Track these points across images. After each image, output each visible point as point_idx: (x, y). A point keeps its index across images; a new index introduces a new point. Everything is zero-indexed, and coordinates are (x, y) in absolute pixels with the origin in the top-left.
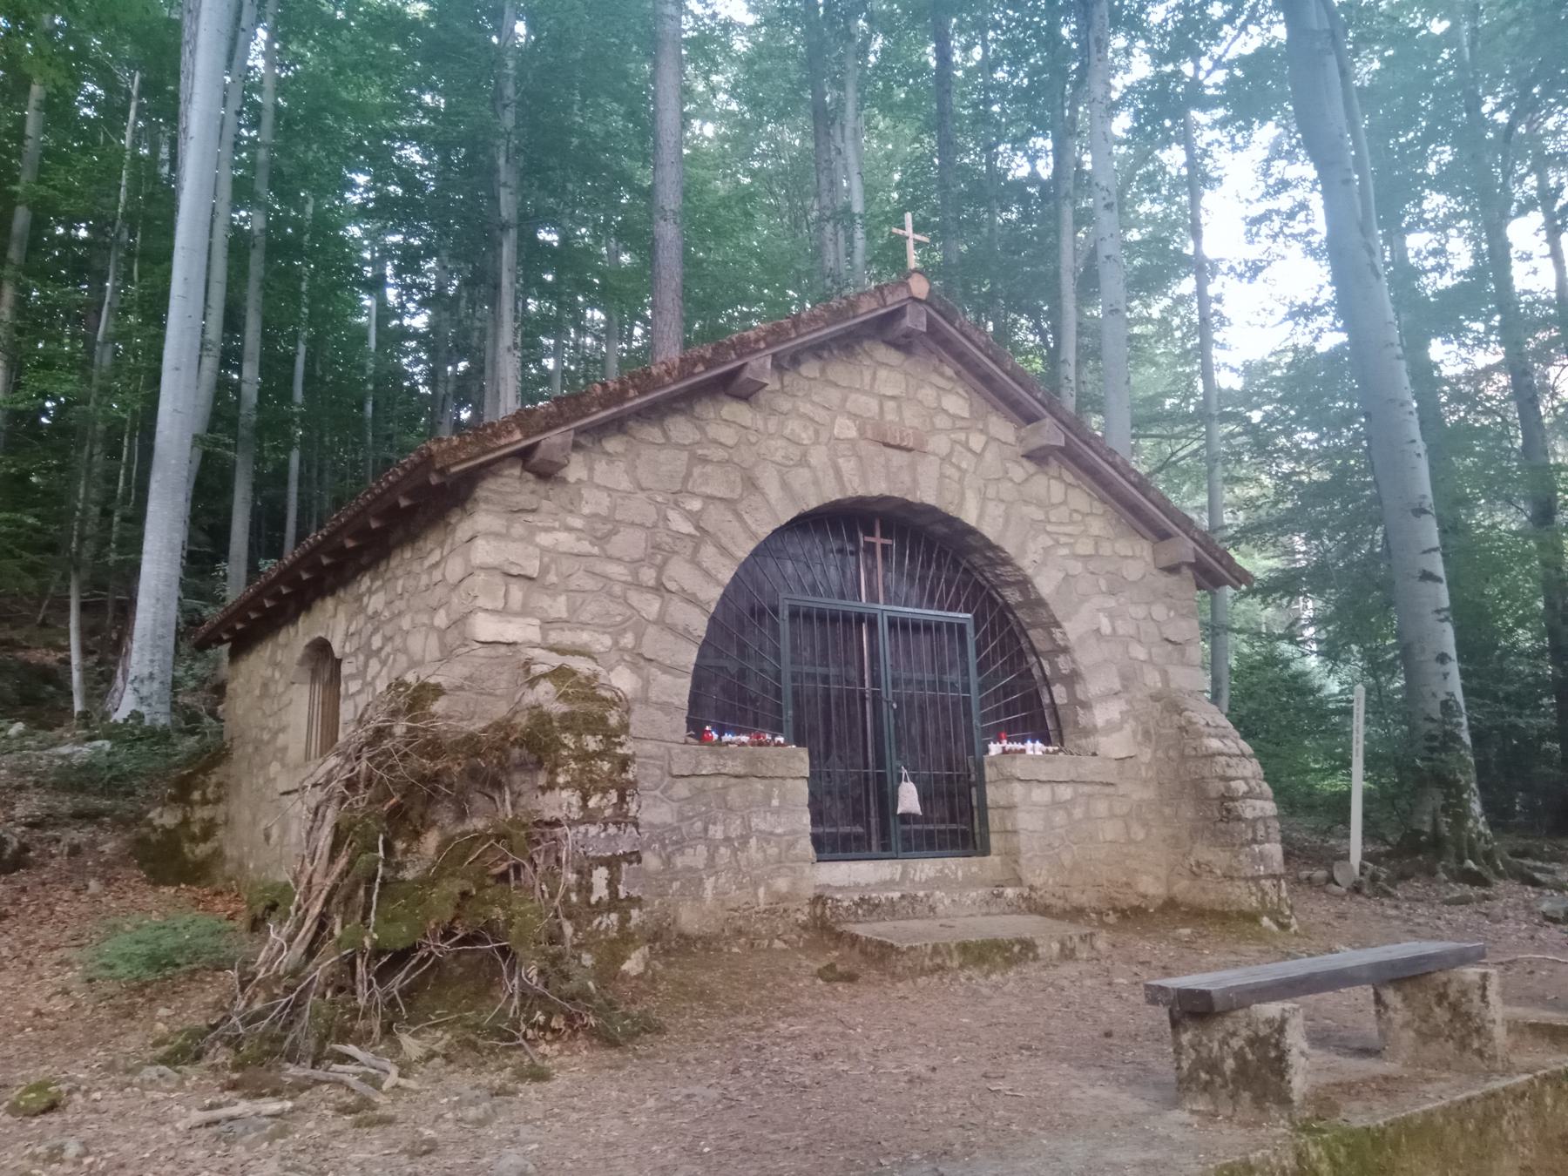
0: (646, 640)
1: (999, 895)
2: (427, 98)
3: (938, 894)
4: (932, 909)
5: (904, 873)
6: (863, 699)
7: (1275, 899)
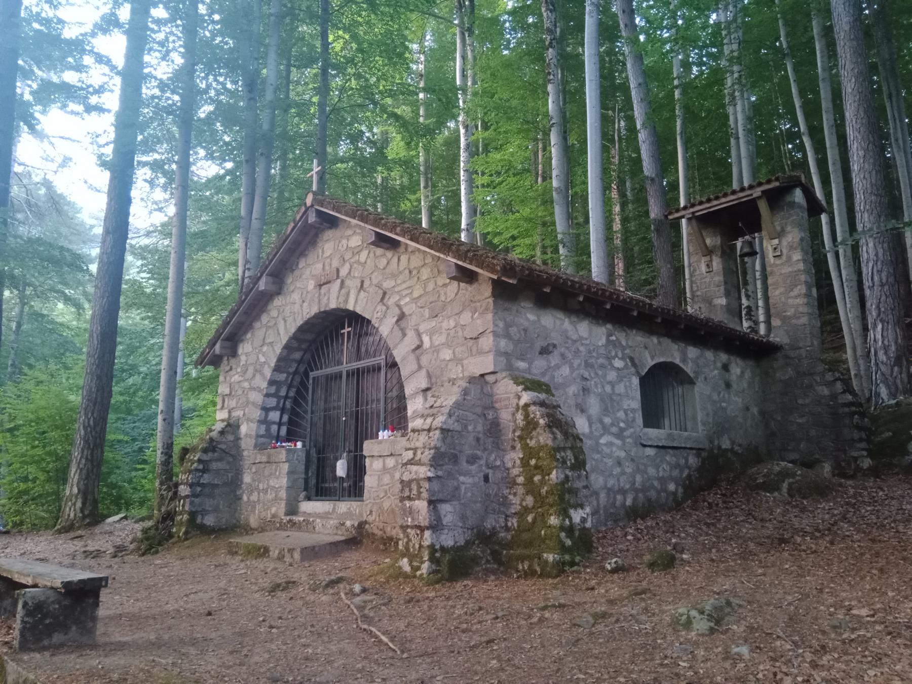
0: (274, 420)
1: (343, 524)
2: (207, 288)
3: (318, 520)
4: (314, 528)
5: (334, 509)
6: (378, 416)
7: (417, 546)
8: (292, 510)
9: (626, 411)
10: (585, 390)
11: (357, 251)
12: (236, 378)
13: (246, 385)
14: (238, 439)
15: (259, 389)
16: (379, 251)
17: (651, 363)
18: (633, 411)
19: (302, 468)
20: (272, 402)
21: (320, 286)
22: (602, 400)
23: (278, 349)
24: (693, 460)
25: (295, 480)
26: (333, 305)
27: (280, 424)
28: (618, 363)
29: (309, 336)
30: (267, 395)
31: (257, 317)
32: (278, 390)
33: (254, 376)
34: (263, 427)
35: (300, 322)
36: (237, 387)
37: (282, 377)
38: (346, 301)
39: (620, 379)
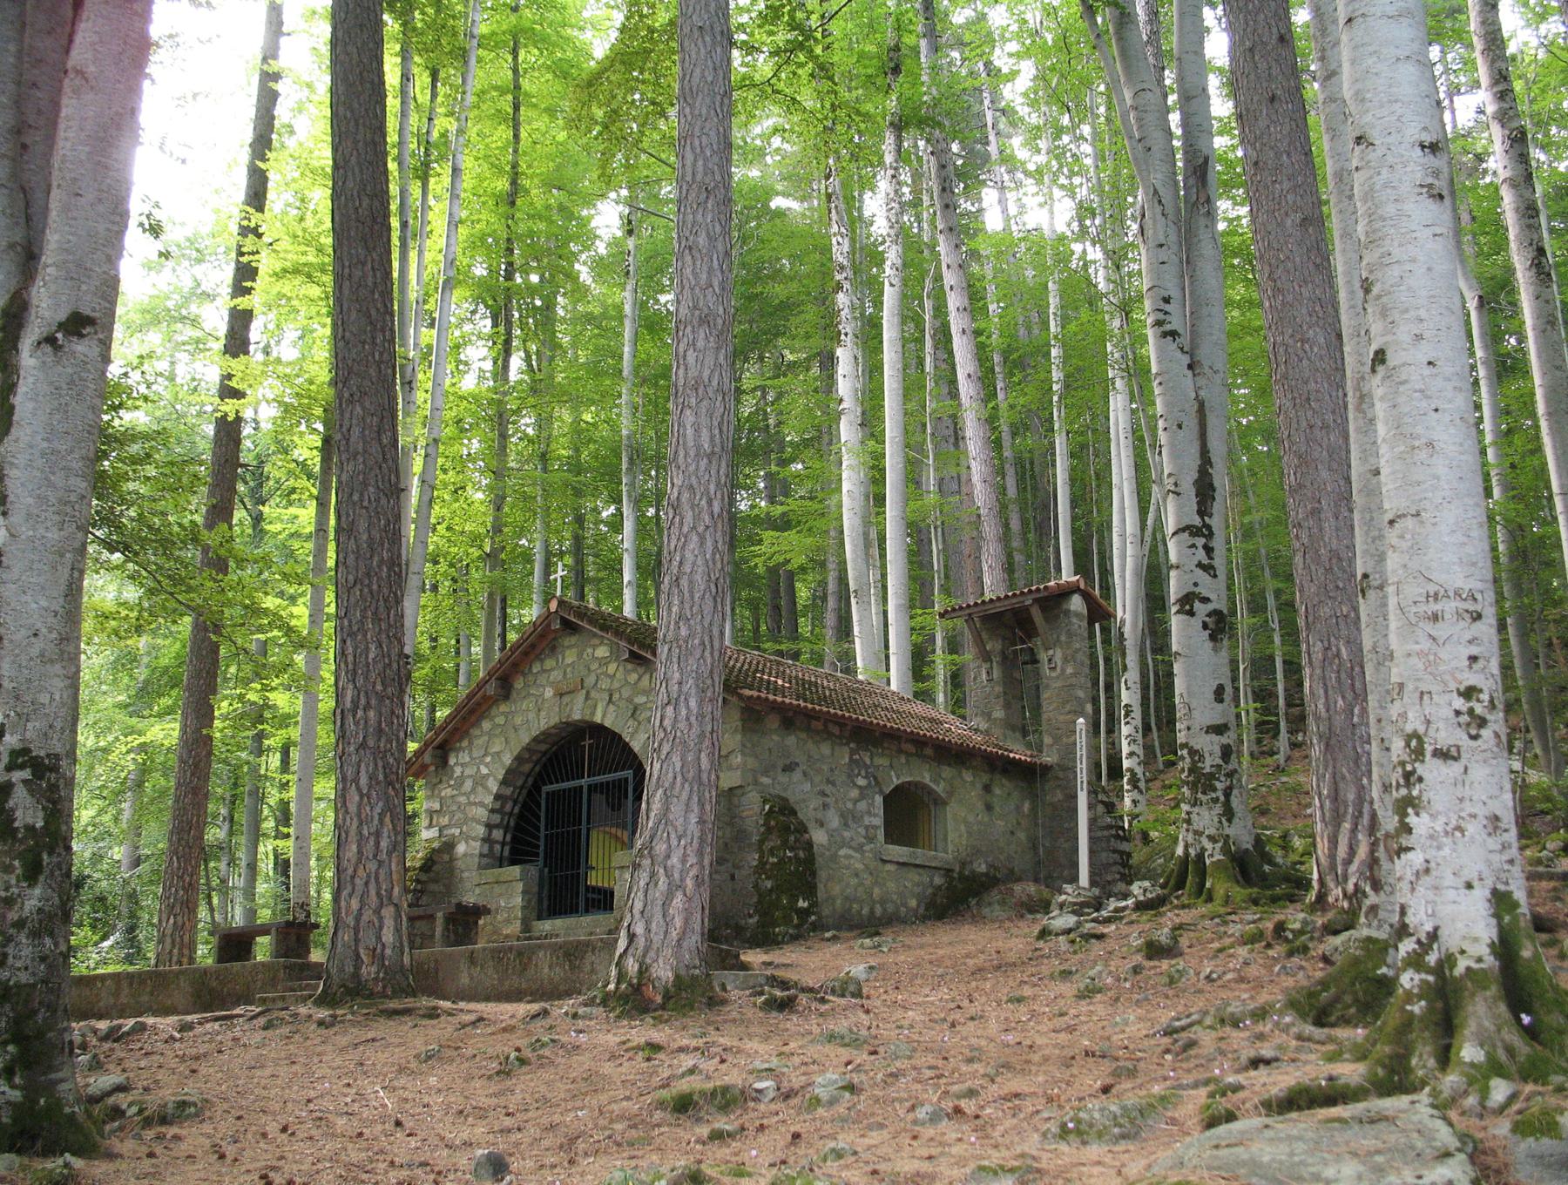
8: (526, 927)
9: (867, 828)
10: (825, 806)
11: (604, 662)
12: (448, 792)
13: (463, 799)
14: (452, 860)
15: (482, 804)
16: (629, 666)
17: (896, 782)
18: (877, 827)
19: (536, 889)
20: (496, 818)
21: (561, 695)
22: (842, 816)
23: (507, 760)
24: (938, 880)
25: (529, 901)
26: (577, 716)
27: (503, 844)
28: (861, 782)
29: (543, 747)
30: (492, 811)
31: (477, 723)
32: (503, 806)
33: (473, 789)
34: (486, 847)
35: (535, 733)
36: (449, 802)
37: (508, 791)
38: (593, 714)
39: (862, 797)
